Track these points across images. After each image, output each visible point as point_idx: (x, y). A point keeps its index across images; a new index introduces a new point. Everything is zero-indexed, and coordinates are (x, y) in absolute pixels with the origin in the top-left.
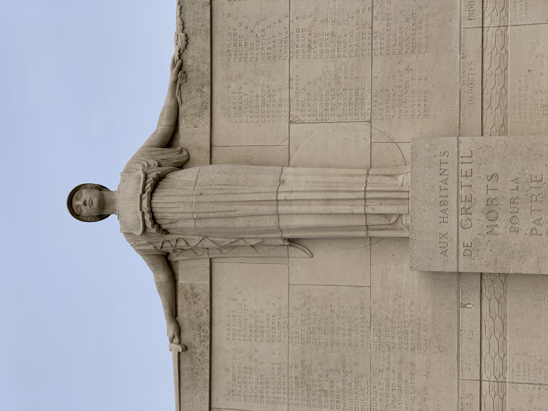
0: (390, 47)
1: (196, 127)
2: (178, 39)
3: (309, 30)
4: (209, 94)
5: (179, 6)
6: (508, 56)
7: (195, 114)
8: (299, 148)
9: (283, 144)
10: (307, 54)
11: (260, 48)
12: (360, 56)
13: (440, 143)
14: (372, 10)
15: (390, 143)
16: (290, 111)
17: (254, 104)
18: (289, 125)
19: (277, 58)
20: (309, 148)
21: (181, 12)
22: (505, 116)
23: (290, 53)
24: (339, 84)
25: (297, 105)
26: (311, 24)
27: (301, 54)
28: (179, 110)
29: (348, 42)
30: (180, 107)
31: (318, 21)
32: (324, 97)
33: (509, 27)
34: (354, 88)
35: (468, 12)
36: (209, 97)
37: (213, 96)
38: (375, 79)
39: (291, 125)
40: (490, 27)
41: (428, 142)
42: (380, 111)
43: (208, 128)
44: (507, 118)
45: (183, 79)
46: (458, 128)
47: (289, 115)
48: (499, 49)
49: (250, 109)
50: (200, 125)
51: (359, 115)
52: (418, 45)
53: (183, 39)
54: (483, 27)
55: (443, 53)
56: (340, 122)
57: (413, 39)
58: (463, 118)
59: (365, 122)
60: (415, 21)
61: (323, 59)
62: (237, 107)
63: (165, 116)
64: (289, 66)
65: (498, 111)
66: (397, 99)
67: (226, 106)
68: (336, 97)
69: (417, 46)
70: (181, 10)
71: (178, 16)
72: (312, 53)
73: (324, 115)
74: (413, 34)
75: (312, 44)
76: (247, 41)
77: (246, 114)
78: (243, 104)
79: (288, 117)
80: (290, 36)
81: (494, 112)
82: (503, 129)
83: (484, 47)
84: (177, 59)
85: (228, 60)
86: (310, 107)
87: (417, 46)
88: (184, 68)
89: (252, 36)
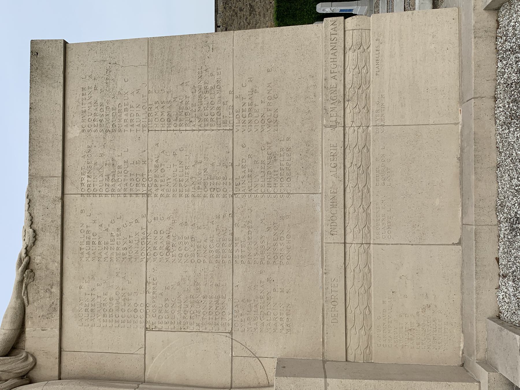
0: (251, 256)
1: (44, 330)
2: (25, 235)
3: (167, 232)
4: (59, 295)
5: (28, 200)
6: (371, 275)
7: (43, 316)
8: (156, 358)
9: (138, 352)
10: (164, 256)
11: (115, 248)
12: (221, 262)
13: (307, 385)
14: (233, 217)
15: (252, 358)
16: (146, 317)
17: (107, 307)
18: (145, 332)
19: (133, 260)
20: (166, 358)
21: (29, 206)
22: (370, 337)
23: (147, 255)
24: (198, 291)
25: (154, 311)
26: (170, 226)
27: (158, 256)
28: (26, 310)
29: (208, 247)
30: (26, 308)
31: (177, 223)
32: (182, 303)
33: (371, 245)
34: (214, 296)
35: (329, 227)
36: (59, 298)
37: (64, 296)
38: (236, 288)
39: (147, 332)
40: (352, 244)
41: (294, 382)
42: (242, 322)
43: (57, 331)
44: (371, 339)
45: (30, 278)
46: (321, 346)
47: (146, 321)
48: (362, 267)
49: (103, 313)
50: (48, 328)
51: (220, 325)
52: (280, 256)
53: (31, 236)
54: (345, 243)
55: (305, 266)
56: (200, 332)
57: (275, 249)
58: (327, 337)
59: (226, 333)
60: (276, 231)
61: (182, 264)
62: (89, 310)
63: (9, 319)
64: (146, 269)
65: (363, 332)
66: (259, 311)
67: (77, 308)
68: (196, 305)
69: (279, 257)
70: (30, 204)
71: (26, 210)
72: (170, 256)
73: (182, 323)
74: (275, 244)
75: (171, 246)
76: (101, 240)
77: (99, 318)
78: (96, 306)
79: (144, 323)
80: (147, 237)
81: (358, 333)
82: (367, 351)
83: (347, 264)
84: (24, 257)
85: (81, 259)
86: (168, 314)
87: (279, 257)
88: (31, 267)
89: (106, 235)
